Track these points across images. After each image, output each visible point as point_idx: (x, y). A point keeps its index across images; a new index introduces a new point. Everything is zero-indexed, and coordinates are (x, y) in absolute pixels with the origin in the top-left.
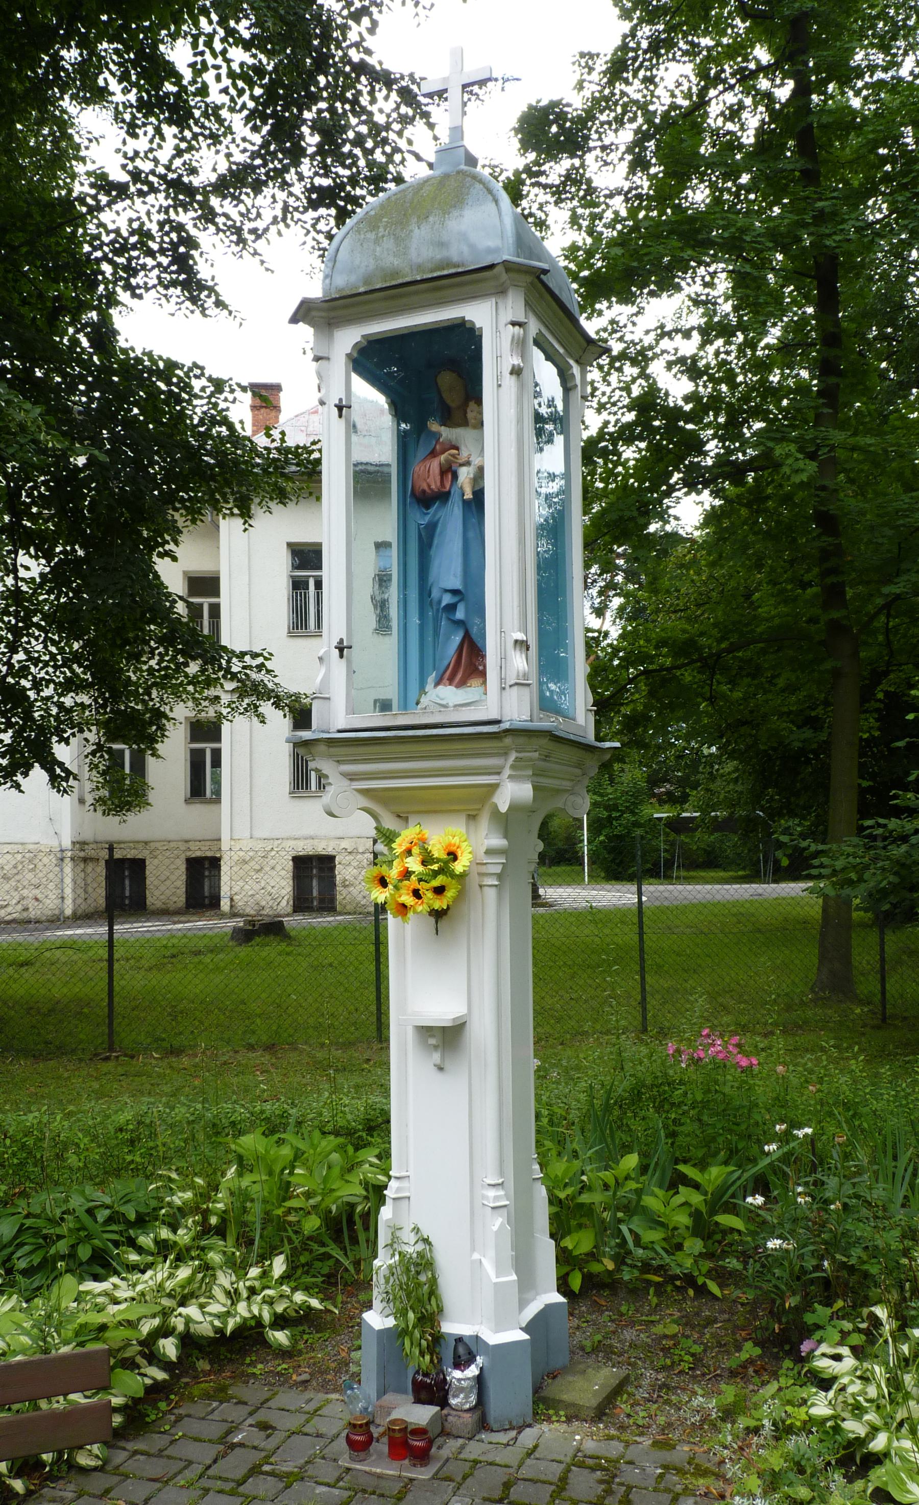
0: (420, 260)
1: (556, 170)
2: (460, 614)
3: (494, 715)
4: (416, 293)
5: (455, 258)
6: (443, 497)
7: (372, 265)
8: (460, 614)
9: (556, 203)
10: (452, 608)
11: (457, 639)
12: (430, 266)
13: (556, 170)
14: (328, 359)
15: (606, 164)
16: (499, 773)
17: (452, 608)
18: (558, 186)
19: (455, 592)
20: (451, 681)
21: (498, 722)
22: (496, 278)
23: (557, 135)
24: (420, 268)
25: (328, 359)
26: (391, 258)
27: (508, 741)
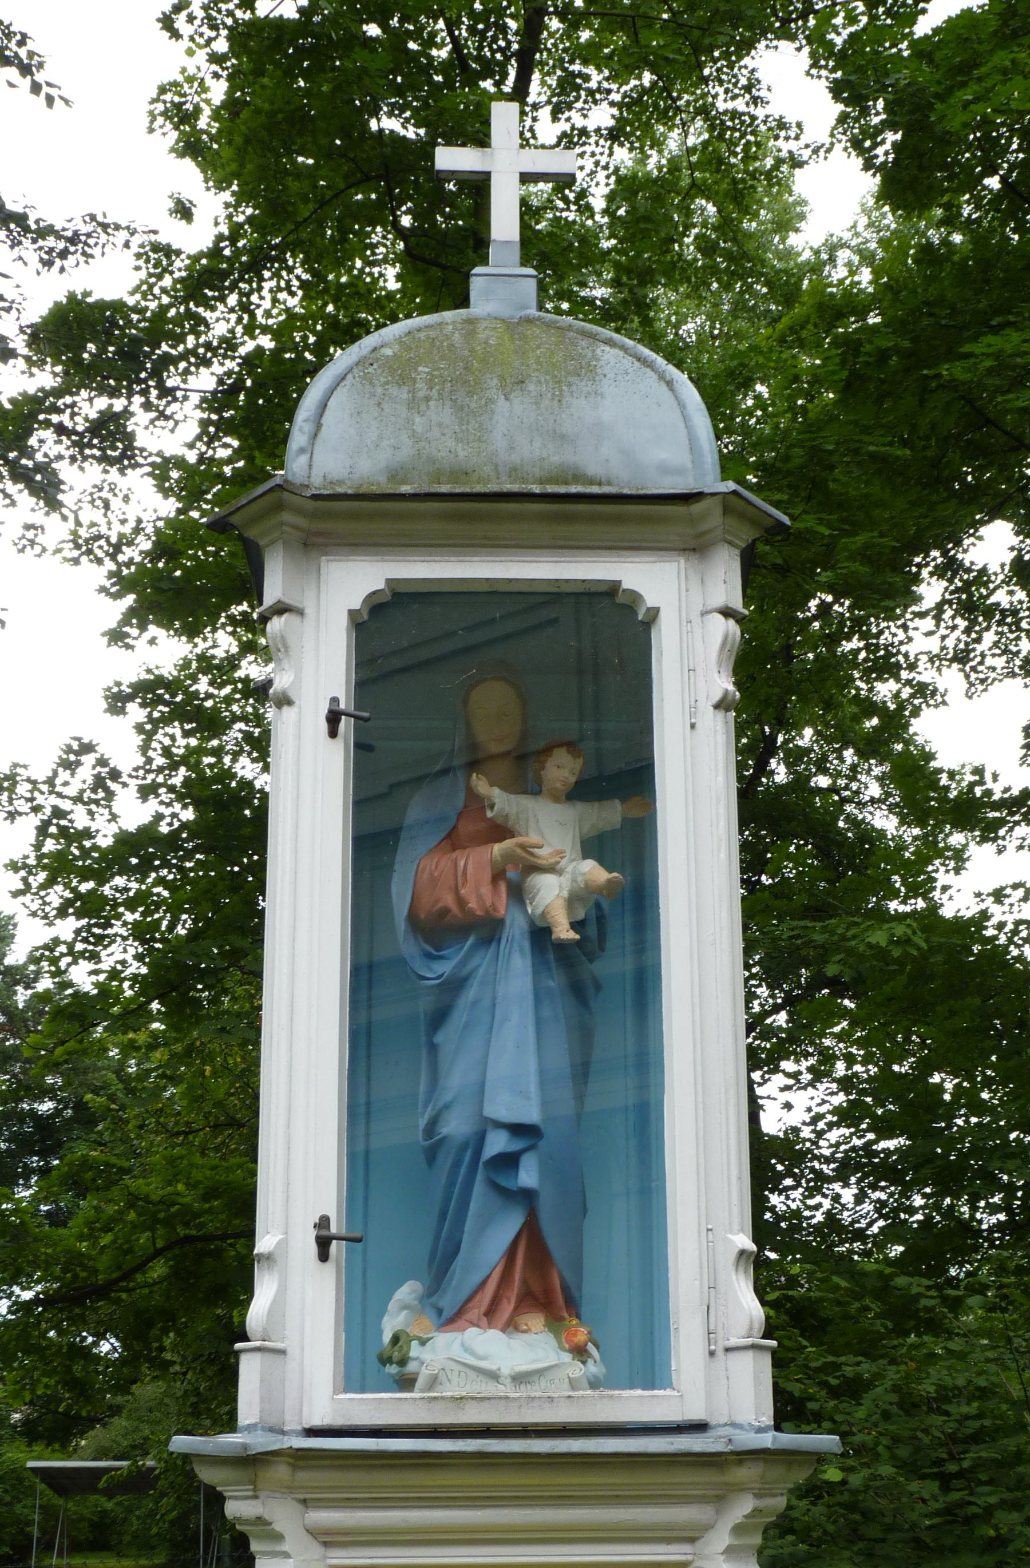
0: (515, 458)
1: (90, 406)
2: (528, 1176)
3: (694, 1413)
4: (514, 517)
5: (593, 469)
6: (489, 930)
7: (407, 450)
8: (528, 1176)
9: (73, 459)
10: (509, 1161)
11: (508, 1227)
12: (537, 472)
13: (90, 406)
14: (300, 612)
15: (162, 415)
16: (692, 1540)
17: (509, 1161)
18: (81, 435)
19: (518, 1130)
20: (490, 1313)
21: (700, 1427)
22: (692, 521)
23: (315, 324)
24: (514, 471)
25: (300, 612)
26: (451, 443)
27: (744, 1473)
